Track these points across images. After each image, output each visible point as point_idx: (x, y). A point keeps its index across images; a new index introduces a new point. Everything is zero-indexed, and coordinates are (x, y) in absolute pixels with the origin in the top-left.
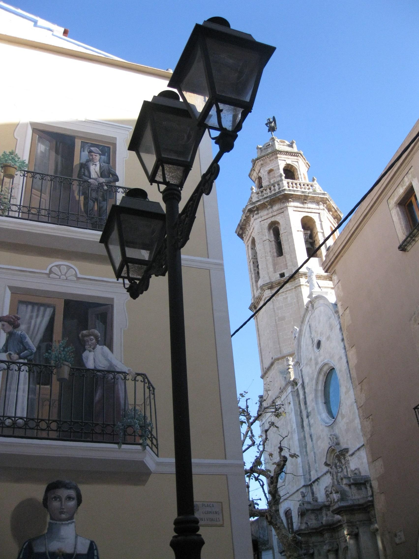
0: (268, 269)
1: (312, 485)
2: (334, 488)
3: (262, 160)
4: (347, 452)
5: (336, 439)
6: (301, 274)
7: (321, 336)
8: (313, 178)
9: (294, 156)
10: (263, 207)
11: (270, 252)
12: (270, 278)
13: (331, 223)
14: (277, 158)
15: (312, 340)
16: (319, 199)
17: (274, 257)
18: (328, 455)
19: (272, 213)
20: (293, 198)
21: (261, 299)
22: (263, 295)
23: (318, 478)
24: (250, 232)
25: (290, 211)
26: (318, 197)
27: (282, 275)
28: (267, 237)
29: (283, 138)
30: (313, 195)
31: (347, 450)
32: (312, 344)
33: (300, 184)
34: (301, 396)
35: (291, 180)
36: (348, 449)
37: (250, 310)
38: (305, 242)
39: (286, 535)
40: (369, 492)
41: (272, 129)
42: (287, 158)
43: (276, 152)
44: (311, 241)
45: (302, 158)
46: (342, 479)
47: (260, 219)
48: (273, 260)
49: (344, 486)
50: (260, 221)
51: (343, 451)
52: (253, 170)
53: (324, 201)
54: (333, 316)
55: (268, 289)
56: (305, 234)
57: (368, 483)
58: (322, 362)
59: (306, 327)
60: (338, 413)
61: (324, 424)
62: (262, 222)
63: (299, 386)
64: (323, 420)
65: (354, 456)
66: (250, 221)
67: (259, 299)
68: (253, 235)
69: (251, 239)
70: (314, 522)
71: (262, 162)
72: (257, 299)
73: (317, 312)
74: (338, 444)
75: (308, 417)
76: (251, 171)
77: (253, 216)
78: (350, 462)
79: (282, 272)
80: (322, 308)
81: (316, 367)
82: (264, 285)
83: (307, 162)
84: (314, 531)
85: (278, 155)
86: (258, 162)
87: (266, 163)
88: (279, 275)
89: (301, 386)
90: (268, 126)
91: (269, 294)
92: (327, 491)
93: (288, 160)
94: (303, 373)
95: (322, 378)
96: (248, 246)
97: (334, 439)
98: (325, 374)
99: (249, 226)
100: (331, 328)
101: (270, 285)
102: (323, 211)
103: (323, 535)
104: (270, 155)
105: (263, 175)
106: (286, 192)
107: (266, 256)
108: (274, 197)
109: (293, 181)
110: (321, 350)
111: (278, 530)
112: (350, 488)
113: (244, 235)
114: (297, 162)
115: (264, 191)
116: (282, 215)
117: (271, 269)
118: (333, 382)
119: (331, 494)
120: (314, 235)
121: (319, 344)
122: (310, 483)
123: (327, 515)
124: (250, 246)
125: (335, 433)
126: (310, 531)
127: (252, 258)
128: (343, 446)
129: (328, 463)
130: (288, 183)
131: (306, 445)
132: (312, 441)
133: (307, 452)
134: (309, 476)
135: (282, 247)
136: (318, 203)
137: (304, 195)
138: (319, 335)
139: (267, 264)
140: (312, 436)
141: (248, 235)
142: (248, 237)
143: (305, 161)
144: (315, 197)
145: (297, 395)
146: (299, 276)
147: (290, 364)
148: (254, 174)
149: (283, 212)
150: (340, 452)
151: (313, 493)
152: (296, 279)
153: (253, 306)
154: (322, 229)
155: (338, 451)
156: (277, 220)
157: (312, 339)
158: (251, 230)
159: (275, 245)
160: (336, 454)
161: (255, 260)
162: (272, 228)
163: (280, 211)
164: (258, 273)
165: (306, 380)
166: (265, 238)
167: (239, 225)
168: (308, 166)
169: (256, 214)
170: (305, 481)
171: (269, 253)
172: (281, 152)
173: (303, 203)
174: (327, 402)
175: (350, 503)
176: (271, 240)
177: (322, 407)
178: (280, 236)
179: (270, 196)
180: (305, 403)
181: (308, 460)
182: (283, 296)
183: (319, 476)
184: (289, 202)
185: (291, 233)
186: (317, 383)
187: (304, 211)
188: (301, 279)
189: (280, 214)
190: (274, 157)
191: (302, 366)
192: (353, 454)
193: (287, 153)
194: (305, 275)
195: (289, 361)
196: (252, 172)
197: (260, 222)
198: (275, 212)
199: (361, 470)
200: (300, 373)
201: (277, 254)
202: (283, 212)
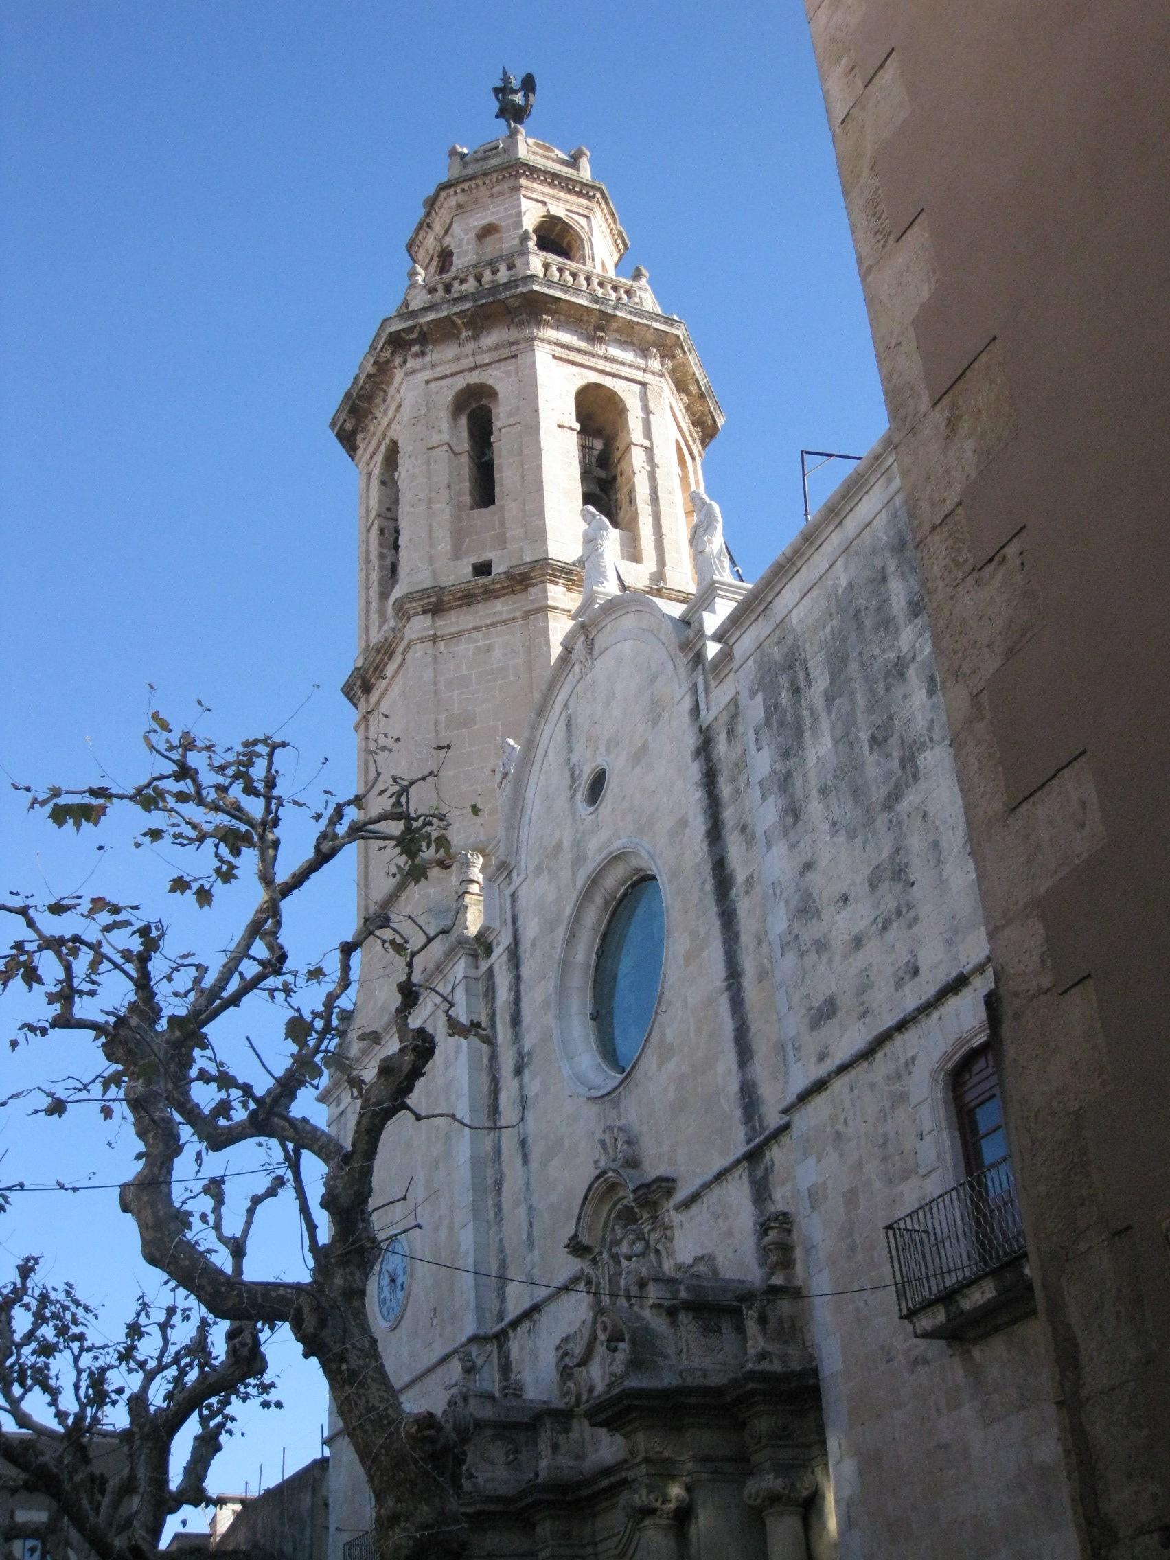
0: (431, 546)
1: (507, 1338)
2: (604, 1319)
3: (463, 190)
4: (669, 1193)
5: (629, 1142)
6: (553, 569)
7: (608, 751)
8: (638, 269)
9: (579, 194)
10: (444, 331)
11: (449, 487)
12: (434, 574)
13: (681, 430)
14: (518, 188)
15: (572, 775)
16: (650, 336)
17: (459, 507)
18: (589, 1208)
19: (474, 354)
20: (556, 316)
21: (393, 652)
22: (402, 638)
23: (536, 1308)
24: (385, 421)
25: (542, 355)
26: (647, 326)
27: (483, 569)
28: (445, 437)
29: (546, 141)
30: (629, 317)
31: (666, 1185)
32: (571, 787)
33: (588, 279)
34: (503, 994)
35: (559, 259)
36: (673, 1180)
37: (347, 695)
38: (581, 473)
39: (388, 1416)
40: (750, 1343)
41: (513, 114)
42: (553, 197)
43: (516, 170)
44: (602, 474)
45: (605, 210)
46: (642, 1285)
47: (427, 374)
48: (457, 519)
49: (647, 1313)
50: (427, 378)
51: (654, 1187)
52: (424, 225)
53: (666, 347)
54: (670, 666)
55: (424, 612)
56: (584, 448)
57: (750, 1308)
58: (600, 850)
59: (552, 732)
60: (647, 1041)
61: (583, 1090)
62: (433, 385)
63: (499, 956)
64: (580, 1078)
65: (695, 1209)
66: (389, 383)
67: (385, 653)
68: (394, 432)
69: (383, 448)
70: (502, 1473)
71: (461, 198)
72: (378, 651)
73: (603, 666)
74: (633, 1163)
75: (519, 1071)
76: (420, 228)
77: (405, 362)
78: (677, 1232)
79: (484, 558)
80: (627, 647)
81: (574, 875)
82: (409, 597)
83: (619, 227)
84: (500, 1508)
85: (523, 182)
86: (448, 196)
87: (476, 201)
88: (470, 569)
89: (505, 958)
90: (498, 99)
91: (424, 629)
92: (566, 1354)
93: (555, 202)
94: (522, 903)
95: (593, 916)
96: (370, 475)
97: (620, 1143)
98: (607, 903)
99: (384, 401)
100: (655, 713)
101: (434, 599)
102: (659, 379)
103: (533, 1526)
104: (494, 176)
105: (461, 240)
106: (536, 288)
107: (430, 501)
108: (491, 299)
109: (566, 261)
110: (601, 809)
111: (351, 1384)
112: (674, 1323)
113: (359, 437)
114: (588, 217)
115: (456, 284)
116: (511, 366)
117: (445, 546)
118: (635, 933)
119: (579, 1365)
120: (617, 455)
121: (598, 783)
122: (498, 1328)
123: (555, 1448)
124: (376, 472)
125: (623, 1122)
126: (479, 1507)
127: (378, 516)
128: (653, 1169)
129: (585, 1240)
130: (546, 266)
131: (499, 1183)
132: (525, 1161)
133: (498, 1208)
134: (497, 1302)
135: (496, 476)
136: (644, 352)
137: (600, 311)
138: (602, 750)
139: (430, 526)
140: (529, 1142)
141: (374, 434)
142: (374, 442)
143: (615, 223)
144: (638, 324)
145: (486, 994)
146: (544, 575)
147: (472, 877)
148: (425, 242)
149: (516, 356)
150: (640, 1192)
151: (506, 1368)
152: (533, 585)
153: (359, 683)
154: (648, 434)
155: (631, 1187)
156: (490, 382)
157: (571, 769)
158: (390, 413)
159: (470, 469)
160: (619, 1207)
161: (391, 524)
162: (466, 413)
163: (503, 350)
164: (394, 568)
165: (531, 929)
166: (436, 439)
167: (348, 395)
168: (621, 246)
169: (416, 355)
170: (480, 1321)
171: (445, 493)
172: (533, 171)
173: (591, 339)
174: (602, 1016)
175: (668, 1380)
176: (457, 449)
177: (580, 1030)
178: (493, 439)
179: (474, 296)
180: (516, 1020)
181: (501, 1240)
182: (476, 641)
183: (537, 1300)
184: (539, 323)
185: (534, 429)
186: (572, 936)
187: (591, 364)
188: (550, 587)
189: (502, 364)
190: (505, 186)
191: (517, 880)
192: (694, 1198)
193: (553, 179)
194: (568, 573)
195: (468, 867)
196: (422, 233)
197: (427, 382)
198: (486, 355)
199: (720, 1261)
200: (508, 905)
201: (474, 500)
202: (516, 356)
